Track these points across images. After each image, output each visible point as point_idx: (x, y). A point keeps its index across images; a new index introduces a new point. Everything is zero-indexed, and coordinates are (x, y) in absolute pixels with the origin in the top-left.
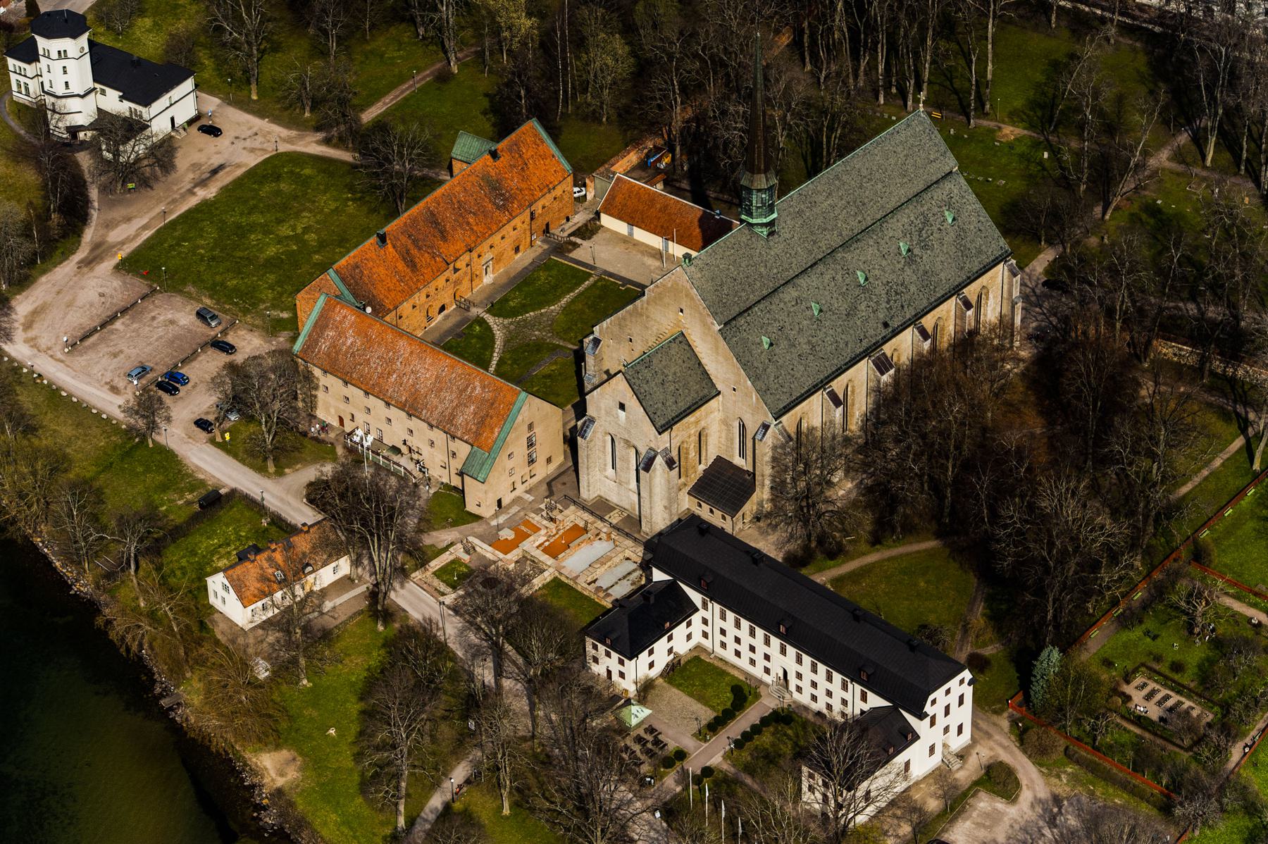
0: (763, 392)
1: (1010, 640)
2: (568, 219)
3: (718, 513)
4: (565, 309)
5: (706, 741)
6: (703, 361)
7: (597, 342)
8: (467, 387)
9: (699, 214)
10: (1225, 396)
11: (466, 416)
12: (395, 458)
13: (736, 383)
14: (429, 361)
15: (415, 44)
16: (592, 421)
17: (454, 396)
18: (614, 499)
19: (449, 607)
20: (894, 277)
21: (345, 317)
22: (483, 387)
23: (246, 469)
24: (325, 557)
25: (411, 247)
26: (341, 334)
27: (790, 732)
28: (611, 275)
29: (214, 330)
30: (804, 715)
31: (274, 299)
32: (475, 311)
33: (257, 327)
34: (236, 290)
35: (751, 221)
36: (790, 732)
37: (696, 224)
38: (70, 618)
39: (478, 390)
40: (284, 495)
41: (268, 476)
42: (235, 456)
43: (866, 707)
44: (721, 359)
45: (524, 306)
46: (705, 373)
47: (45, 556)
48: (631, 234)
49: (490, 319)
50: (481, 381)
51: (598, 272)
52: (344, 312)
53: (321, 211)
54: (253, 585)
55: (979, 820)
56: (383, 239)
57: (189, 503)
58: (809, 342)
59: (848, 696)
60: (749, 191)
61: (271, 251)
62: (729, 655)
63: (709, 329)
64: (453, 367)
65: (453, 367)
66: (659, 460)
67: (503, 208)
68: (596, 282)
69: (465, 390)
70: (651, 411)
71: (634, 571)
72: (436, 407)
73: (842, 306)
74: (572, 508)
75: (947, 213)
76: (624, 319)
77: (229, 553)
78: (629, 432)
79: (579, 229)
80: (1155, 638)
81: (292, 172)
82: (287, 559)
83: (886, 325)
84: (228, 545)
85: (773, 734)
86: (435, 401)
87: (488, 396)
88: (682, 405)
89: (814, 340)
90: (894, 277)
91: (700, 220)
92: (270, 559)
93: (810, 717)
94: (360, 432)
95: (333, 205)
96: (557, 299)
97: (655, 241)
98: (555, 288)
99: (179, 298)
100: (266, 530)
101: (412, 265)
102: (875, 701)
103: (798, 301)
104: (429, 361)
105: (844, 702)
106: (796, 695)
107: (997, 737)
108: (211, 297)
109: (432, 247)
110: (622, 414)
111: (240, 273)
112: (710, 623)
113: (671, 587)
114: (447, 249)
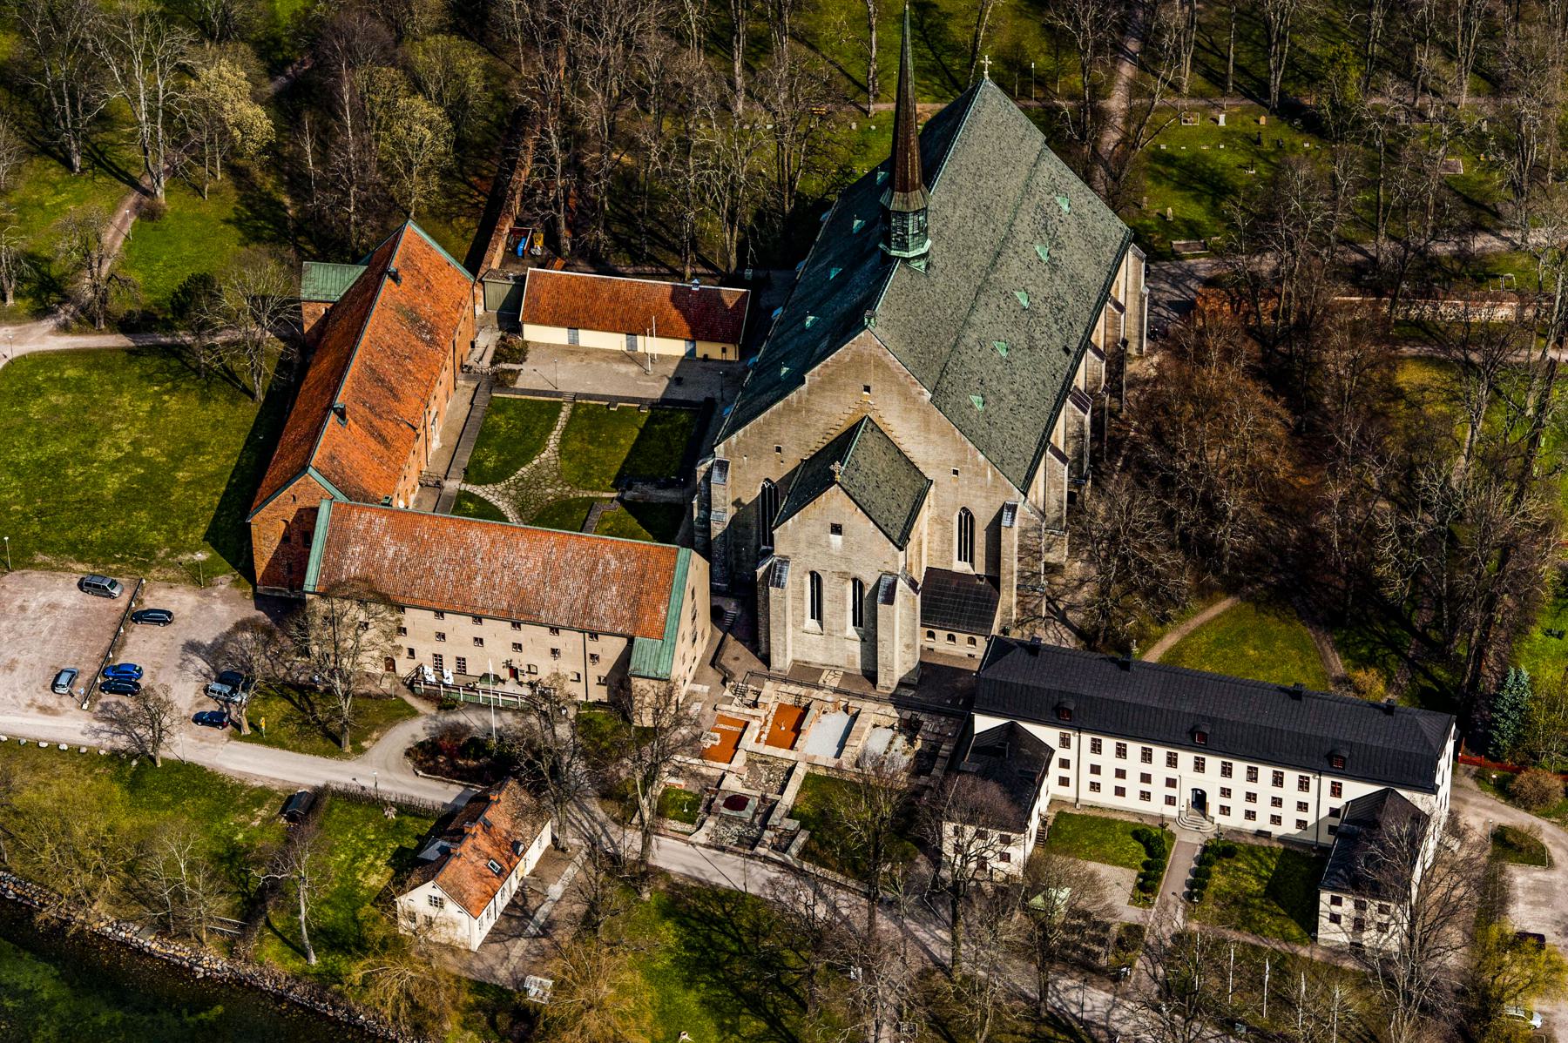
0: (999, 465)
1: (1400, 686)
2: (473, 344)
3: (962, 638)
4: (561, 451)
5: (1151, 906)
6: (902, 448)
7: (723, 466)
8: (596, 563)
9: (668, 291)
10: (1425, 343)
11: (609, 601)
12: (499, 687)
13: (959, 462)
14: (523, 545)
15: (76, 180)
16: (785, 561)
17: (580, 580)
18: (817, 658)
19: (708, 846)
20: (1047, 290)
21: (371, 522)
22: (621, 558)
23: (306, 756)
24: (529, 828)
25: (371, 417)
26: (373, 546)
27: (1240, 865)
28: (589, 397)
29: (122, 598)
30: (1242, 840)
31: (168, 541)
32: (453, 485)
33: (176, 581)
34: (106, 543)
35: (906, 255)
36: (1240, 865)
37: (670, 305)
38: (220, 1009)
39: (614, 564)
40: (382, 769)
41: (347, 757)
42: (283, 746)
43: (1338, 803)
44: (933, 437)
45: (506, 463)
46: (910, 463)
47: (125, 944)
48: (574, 340)
49: (478, 490)
50: (613, 552)
51: (569, 398)
52: (366, 516)
53: (137, 418)
54: (475, 889)
55: (1531, 898)
56: (342, 414)
57: (268, 821)
58: (1012, 392)
59: (1309, 797)
60: (903, 215)
61: (113, 483)
62: (1106, 798)
63: (915, 401)
64: (563, 544)
65: (563, 544)
66: (902, 585)
67: (432, 343)
68: (574, 410)
69: (594, 568)
70: (882, 523)
71: (894, 737)
72: (560, 602)
73: (1020, 338)
74: (769, 684)
75: (1059, 200)
76: (768, 423)
77: (372, 865)
78: (848, 560)
79: (496, 353)
80: (1560, 636)
81: (50, 379)
82: (495, 844)
83: (1067, 351)
84: (363, 856)
85: (1224, 873)
86: (555, 595)
87: (632, 567)
88: (906, 508)
89: (1015, 386)
90: (1047, 290)
91: (673, 298)
92: (475, 849)
93: (1250, 840)
94: (429, 670)
95: (146, 406)
96: (540, 446)
97: (615, 341)
98: (527, 430)
99: (35, 575)
100: (398, 824)
101: (382, 439)
102: (1355, 790)
103: (981, 343)
104: (523, 545)
105: (1303, 806)
106: (1221, 820)
107: (1473, 800)
108: (80, 560)
109: (390, 412)
110: (836, 540)
111: (94, 521)
112: (1073, 764)
113: (1011, 731)
114: (407, 410)
